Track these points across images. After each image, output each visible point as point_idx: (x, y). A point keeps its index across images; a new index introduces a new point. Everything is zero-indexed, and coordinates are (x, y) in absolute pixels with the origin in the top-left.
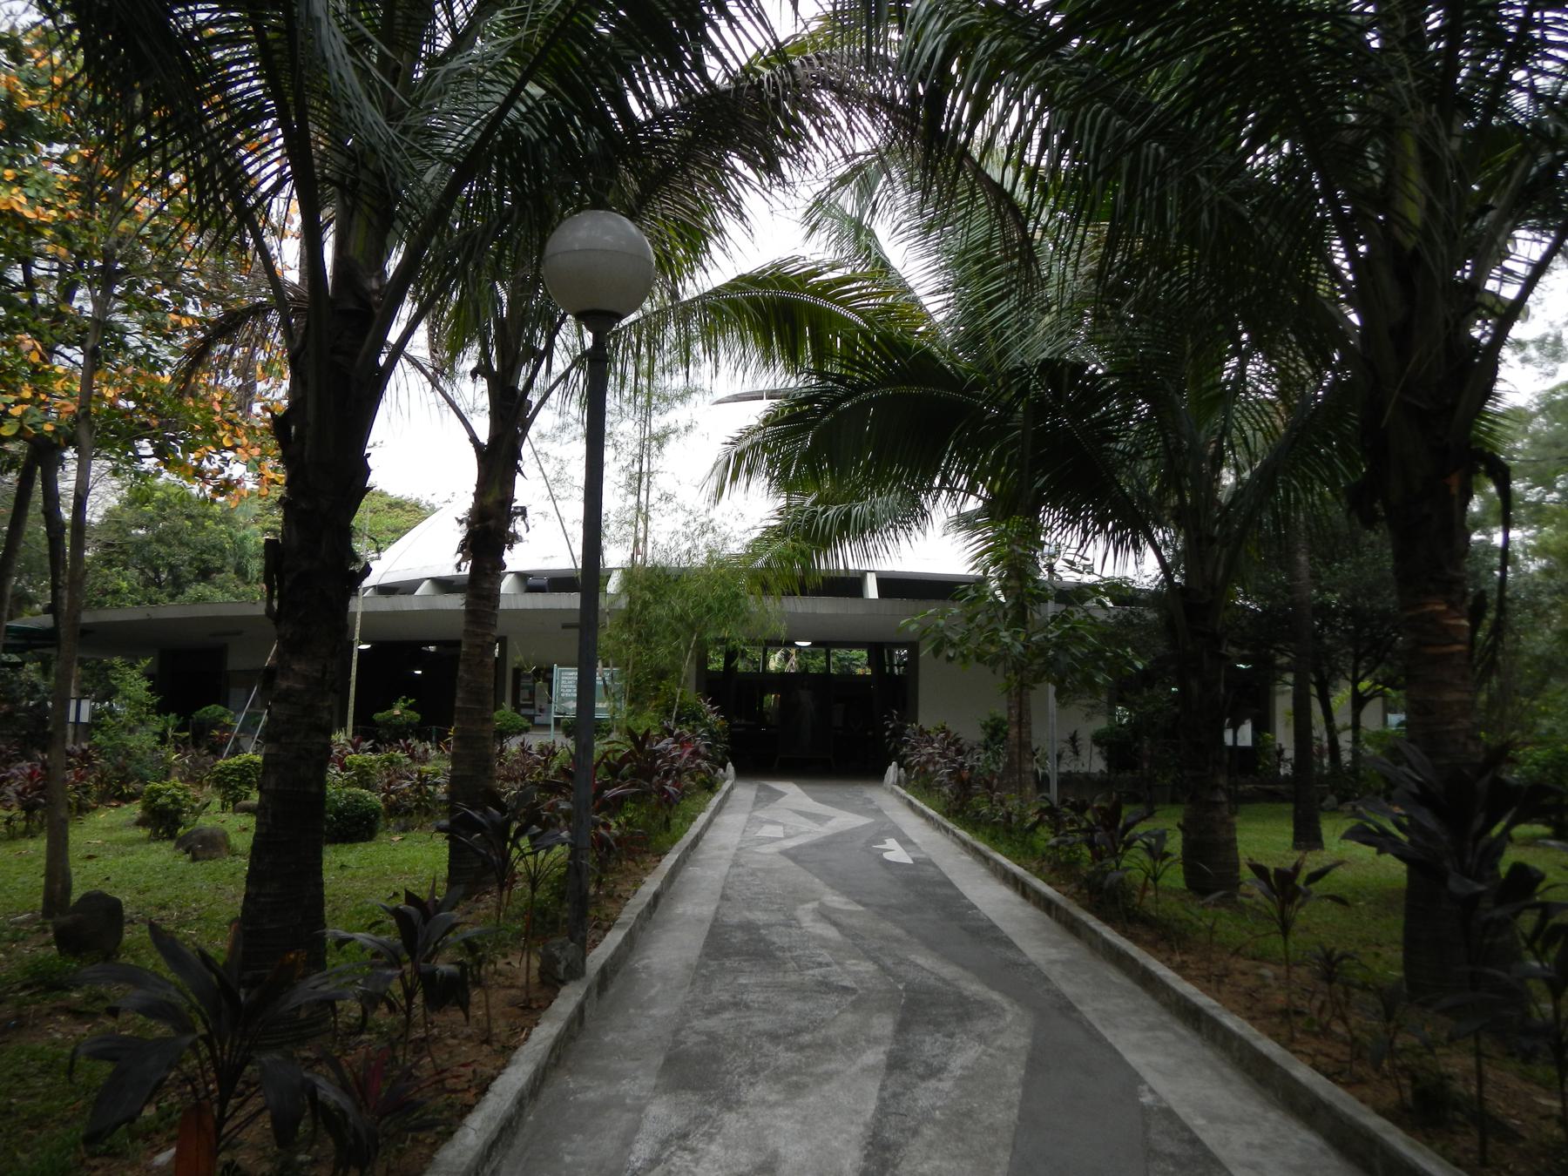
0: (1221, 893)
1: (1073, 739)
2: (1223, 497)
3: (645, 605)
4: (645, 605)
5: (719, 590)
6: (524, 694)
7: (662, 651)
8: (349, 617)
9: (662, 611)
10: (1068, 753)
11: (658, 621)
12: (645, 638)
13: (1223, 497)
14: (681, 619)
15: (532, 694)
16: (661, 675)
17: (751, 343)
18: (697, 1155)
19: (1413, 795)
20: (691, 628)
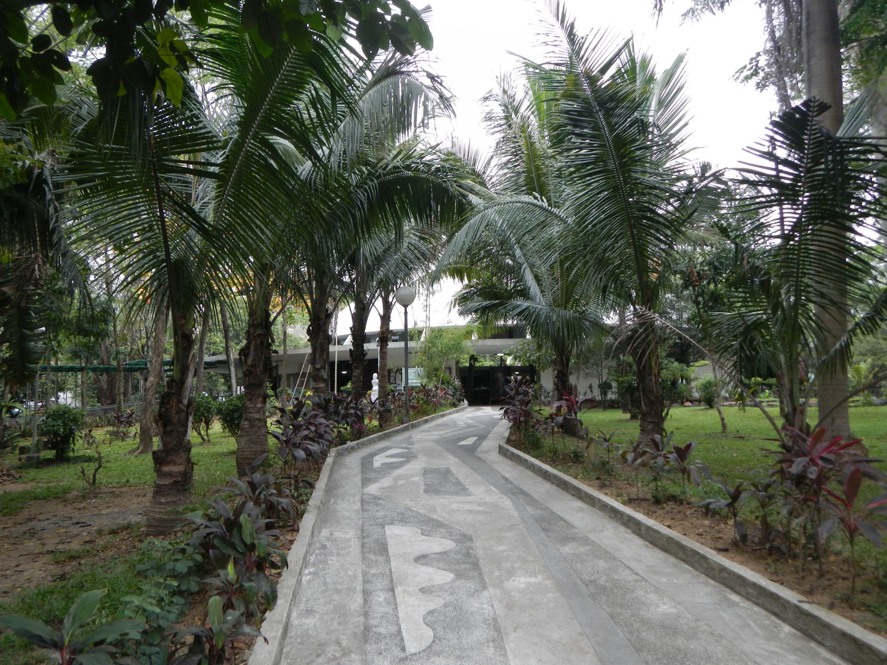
0: (191, 419)
1: (591, 387)
2: (285, 33)
3: (430, 348)
4: (430, 348)
5: (452, 342)
6: (392, 379)
7: (436, 362)
8: (330, 355)
9: (435, 349)
10: (589, 392)
11: (434, 352)
12: (431, 358)
13: (285, 33)
14: (441, 352)
15: (395, 379)
16: (437, 370)
17: (456, 279)
18: (741, 544)
19: (618, 92)
20: (445, 354)
